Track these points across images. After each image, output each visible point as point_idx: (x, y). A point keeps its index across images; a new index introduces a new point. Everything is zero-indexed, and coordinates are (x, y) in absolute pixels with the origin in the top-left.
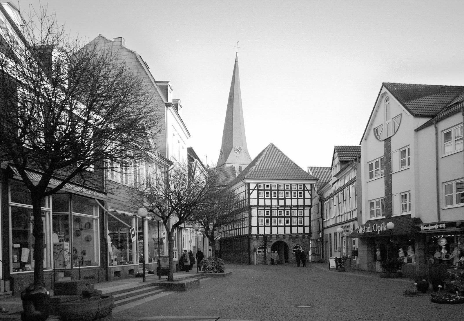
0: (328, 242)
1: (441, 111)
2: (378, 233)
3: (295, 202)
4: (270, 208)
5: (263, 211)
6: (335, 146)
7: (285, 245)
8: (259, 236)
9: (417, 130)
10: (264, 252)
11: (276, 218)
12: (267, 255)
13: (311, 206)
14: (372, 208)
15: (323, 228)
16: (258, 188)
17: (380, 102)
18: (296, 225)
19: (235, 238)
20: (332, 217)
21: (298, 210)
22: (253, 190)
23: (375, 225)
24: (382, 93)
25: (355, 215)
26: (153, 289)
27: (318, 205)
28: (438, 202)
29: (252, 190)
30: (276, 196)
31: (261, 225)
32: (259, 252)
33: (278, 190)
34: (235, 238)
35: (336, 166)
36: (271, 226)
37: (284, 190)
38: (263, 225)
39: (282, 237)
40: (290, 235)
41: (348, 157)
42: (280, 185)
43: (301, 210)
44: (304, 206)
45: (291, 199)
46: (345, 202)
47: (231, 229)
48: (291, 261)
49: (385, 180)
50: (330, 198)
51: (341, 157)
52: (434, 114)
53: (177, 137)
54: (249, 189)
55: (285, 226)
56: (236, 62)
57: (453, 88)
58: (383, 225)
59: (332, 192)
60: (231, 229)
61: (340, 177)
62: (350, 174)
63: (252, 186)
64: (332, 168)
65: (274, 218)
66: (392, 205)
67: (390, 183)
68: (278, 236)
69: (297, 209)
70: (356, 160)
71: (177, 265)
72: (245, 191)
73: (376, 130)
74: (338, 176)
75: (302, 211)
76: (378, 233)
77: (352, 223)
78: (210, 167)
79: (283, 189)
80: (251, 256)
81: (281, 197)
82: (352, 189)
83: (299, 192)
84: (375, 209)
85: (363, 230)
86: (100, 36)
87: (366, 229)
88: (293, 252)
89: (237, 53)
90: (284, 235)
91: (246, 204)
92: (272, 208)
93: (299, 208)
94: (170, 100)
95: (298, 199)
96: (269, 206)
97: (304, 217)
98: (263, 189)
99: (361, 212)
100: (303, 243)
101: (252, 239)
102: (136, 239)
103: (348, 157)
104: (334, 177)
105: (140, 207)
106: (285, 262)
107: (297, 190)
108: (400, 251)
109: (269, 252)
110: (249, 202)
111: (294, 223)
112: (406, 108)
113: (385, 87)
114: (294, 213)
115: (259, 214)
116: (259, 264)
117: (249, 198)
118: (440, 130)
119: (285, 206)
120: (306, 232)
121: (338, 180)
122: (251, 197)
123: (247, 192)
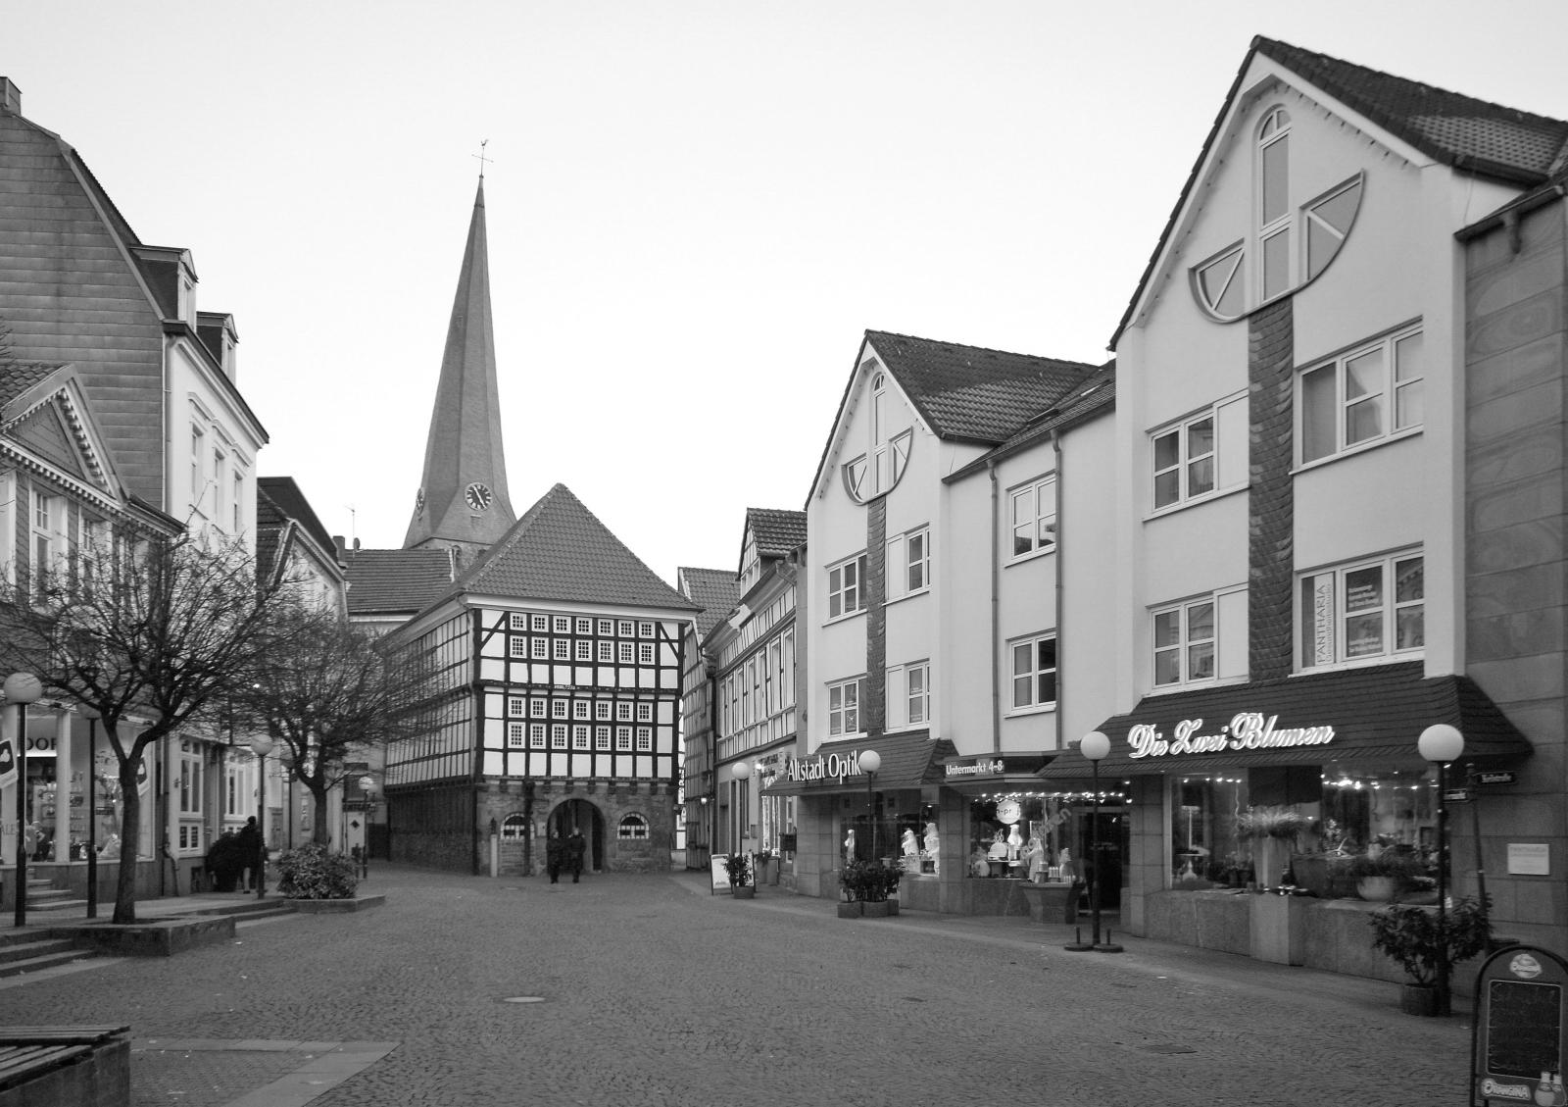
1: (1022, 428)
3: (627, 678)
5: (524, 701)
6: (748, 509)
8: (509, 783)
9: (950, 481)
10: (525, 833)
11: (566, 727)
12: (533, 844)
13: (678, 693)
14: (836, 705)
15: (718, 763)
16: (507, 625)
17: (860, 386)
18: (630, 749)
19: (434, 785)
21: (639, 704)
22: (493, 631)
24: (864, 359)
25: (790, 726)
26: (45, 947)
28: (996, 695)
30: (568, 653)
31: (622, 749)
32: (506, 833)
33: (573, 637)
34: (434, 785)
36: (549, 751)
37: (595, 638)
38: (523, 746)
39: (584, 787)
40: (612, 782)
41: (783, 546)
42: (582, 619)
43: (646, 704)
44: (658, 691)
45: (617, 666)
47: (421, 754)
48: (611, 866)
49: (869, 624)
51: (764, 545)
52: (996, 439)
53: (210, 438)
54: (478, 629)
55: (593, 753)
56: (479, 206)
57: (1062, 366)
59: (740, 651)
60: (421, 754)
61: (757, 602)
62: (783, 599)
63: (489, 619)
64: (740, 575)
67: (880, 631)
68: (572, 782)
69: (636, 701)
70: (794, 554)
71: (195, 870)
72: (467, 632)
73: (848, 468)
74: (752, 602)
75: (651, 706)
77: (781, 749)
78: (363, 547)
79: (590, 633)
80: (482, 844)
81: (582, 659)
83: (640, 645)
84: (843, 710)
85: (803, 772)
87: (810, 769)
88: (619, 837)
89: (481, 177)
90: (592, 782)
91: (462, 676)
92: (554, 694)
93: (641, 697)
94: (185, 315)
96: (543, 687)
97: (655, 725)
98: (525, 629)
99: (805, 717)
100: (651, 809)
101: (485, 790)
102: (17, 778)
103: (783, 546)
105: (14, 670)
106: (594, 869)
107: (637, 640)
108: (904, 839)
109: (539, 834)
110: (477, 669)
112: (923, 411)
115: (510, 709)
116: (507, 872)
117: (478, 658)
118: (1004, 484)
119: (595, 689)
120: (660, 775)
122: (484, 652)
123: (471, 634)
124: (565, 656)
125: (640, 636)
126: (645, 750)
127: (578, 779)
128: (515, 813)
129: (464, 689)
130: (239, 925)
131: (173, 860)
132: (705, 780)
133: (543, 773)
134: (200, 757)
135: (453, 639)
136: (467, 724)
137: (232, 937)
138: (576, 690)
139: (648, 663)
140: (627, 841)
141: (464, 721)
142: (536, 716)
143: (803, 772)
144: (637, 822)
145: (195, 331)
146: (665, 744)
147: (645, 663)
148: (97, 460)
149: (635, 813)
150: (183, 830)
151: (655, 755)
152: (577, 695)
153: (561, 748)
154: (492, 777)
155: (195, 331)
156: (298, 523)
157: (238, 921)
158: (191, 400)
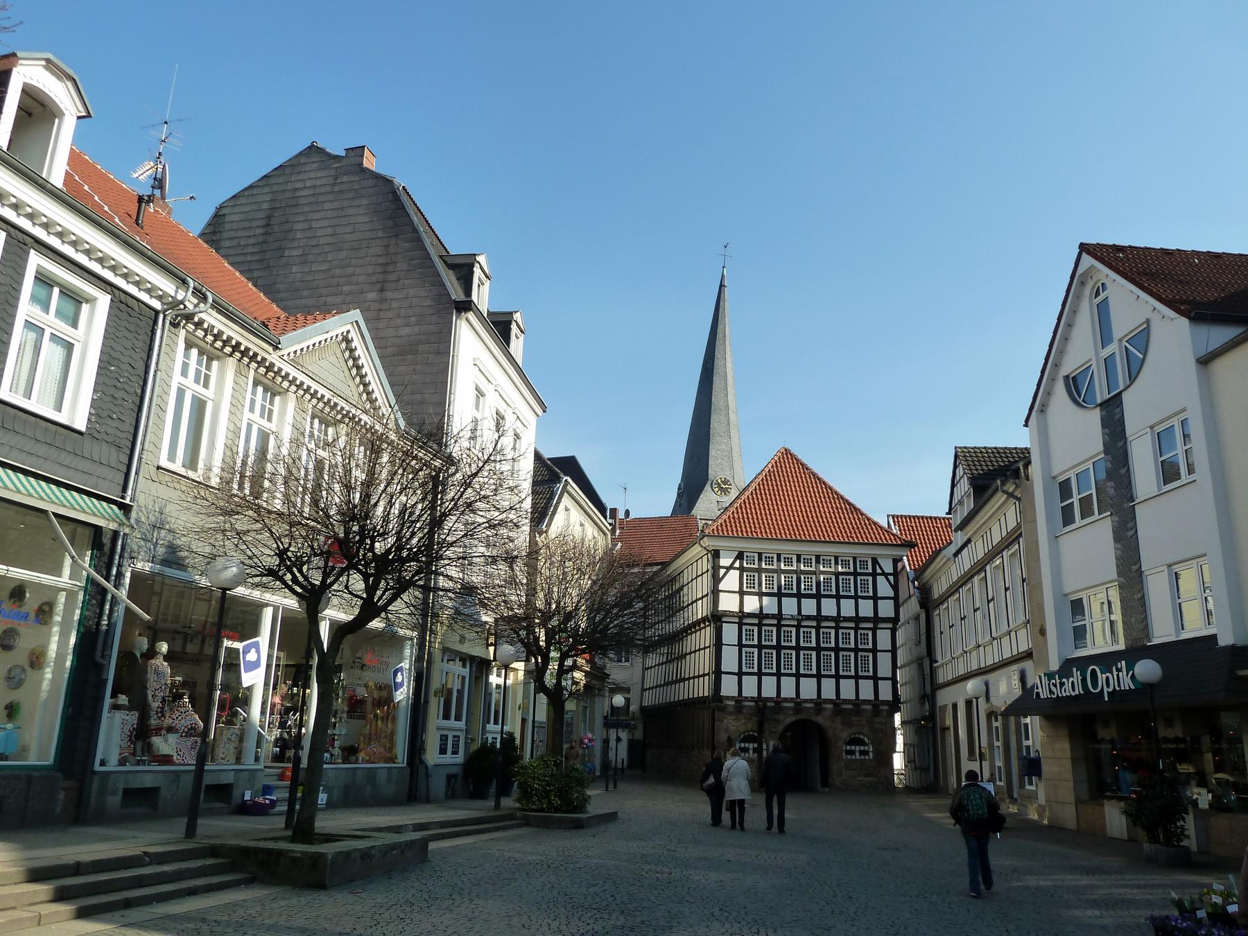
0: (948, 728)
2: (1106, 699)
3: (848, 608)
4: (775, 622)
7: (821, 731)
14: (1079, 617)
16: (741, 564)
17: (1078, 297)
20: (959, 653)
22: (728, 569)
23: (1093, 671)
27: (917, 618)
29: (723, 567)
35: (960, 502)
36: (779, 675)
38: (756, 670)
39: (810, 708)
40: (837, 702)
43: (866, 632)
44: (876, 620)
46: (991, 604)
47: (674, 678)
50: (949, 596)
54: (716, 568)
55: (819, 676)
56: (722, 286)
58: (1119, 670)
59: (955, 578)
61: (971, 529)
65: (786, 651)
66: (1144, 605)
67: (1131, 533)
71: (450, 778)
72: (708, 571)
76: (1106, 699)
78: (632, 516)
82: (1009, 567)
83: (859, 578)
85: (1053, 688)
86: (313, 146)
87: (1062, 684)
90: (819, 702)
91: (701, 610)
92: (783, 622)
95: (856, 597)
96: (773, 616)
97: (874, 651)
99: (1043, 632)
104: (956, 531)
110: (716, 602)
111: (848, 668)
113: (1089, 253)
114: (846, 638)
117: (715, 592)
119: (819, 618)
121: (969, 541)
122: (722, 586)
124: (792, 589)
125: (858, 570)
126: (866, 674)
127: (806, 701)
128: (748, 731)
129: (704, 620)
130: (432, 846)
131: (427, 767)
132: (922, 704)
133: (774, 695)
134: (466, 672)
135: (696, 578)
136: (707, 650)
137: (422, 862)
138: (802, 619)
139: (866, 594)
140: (852, 760)
141: (705, 648)
142: (767, 643)
143: (1053, 688)
144: (862, 743)
145: (485, 315)
146: (884, 669)
147: (863, 594)
148: (376, 394)
149: (860, 734)
150: (444, 739)
151: (875, 679)
152: (804, 623)
153: (789, 671)
154: (728, 698)
155: (485, 315)
156: (570, 480)
157: (431, 840)
158: (475, 365)
